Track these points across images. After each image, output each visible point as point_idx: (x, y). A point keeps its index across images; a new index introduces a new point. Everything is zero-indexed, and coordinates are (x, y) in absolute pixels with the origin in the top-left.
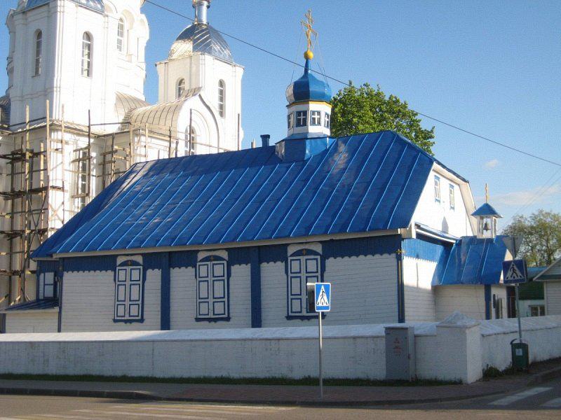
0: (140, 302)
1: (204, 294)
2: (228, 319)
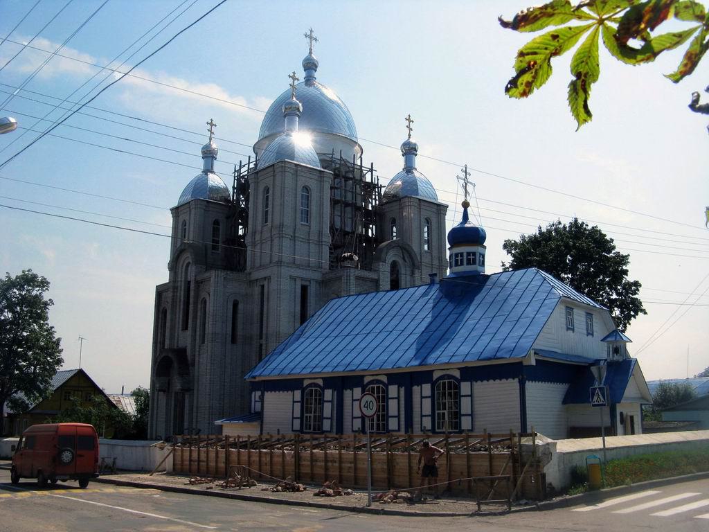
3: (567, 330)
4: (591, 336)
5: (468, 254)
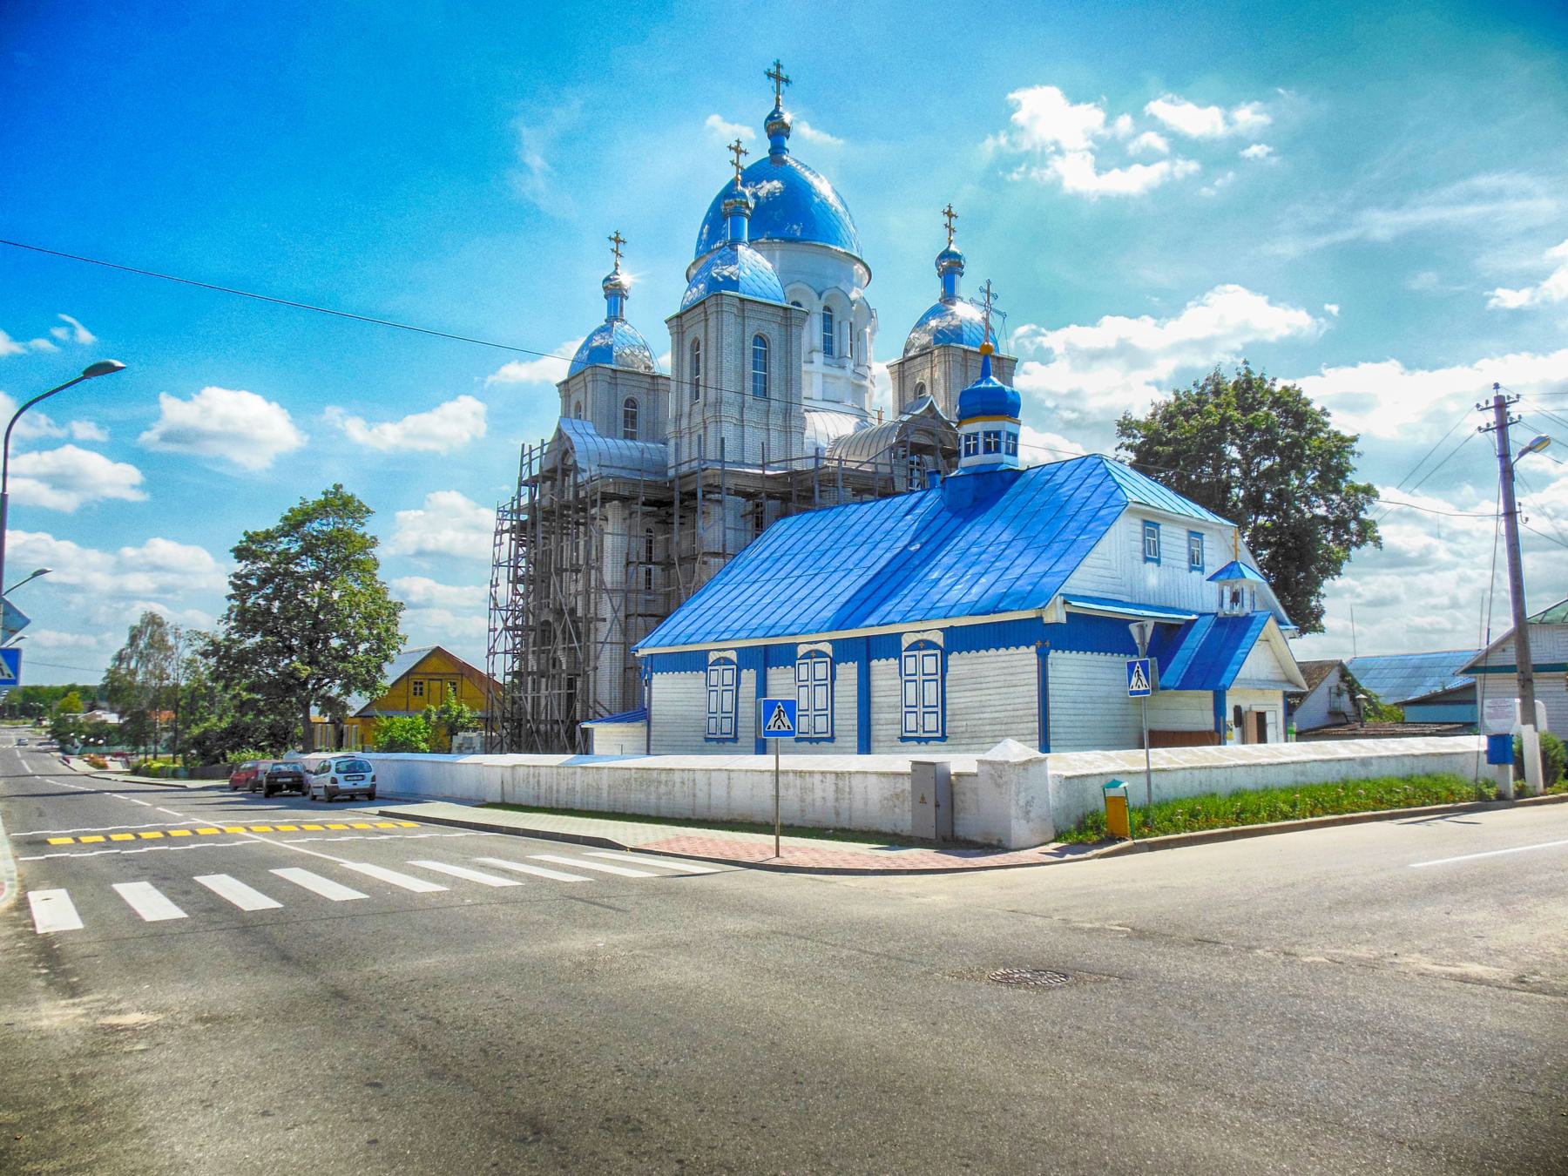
0: (733, 715)
1: (911, 700)
2: (832, 739)
3: (1190, 572)
4: (1155, 565)
5: (987, 434)
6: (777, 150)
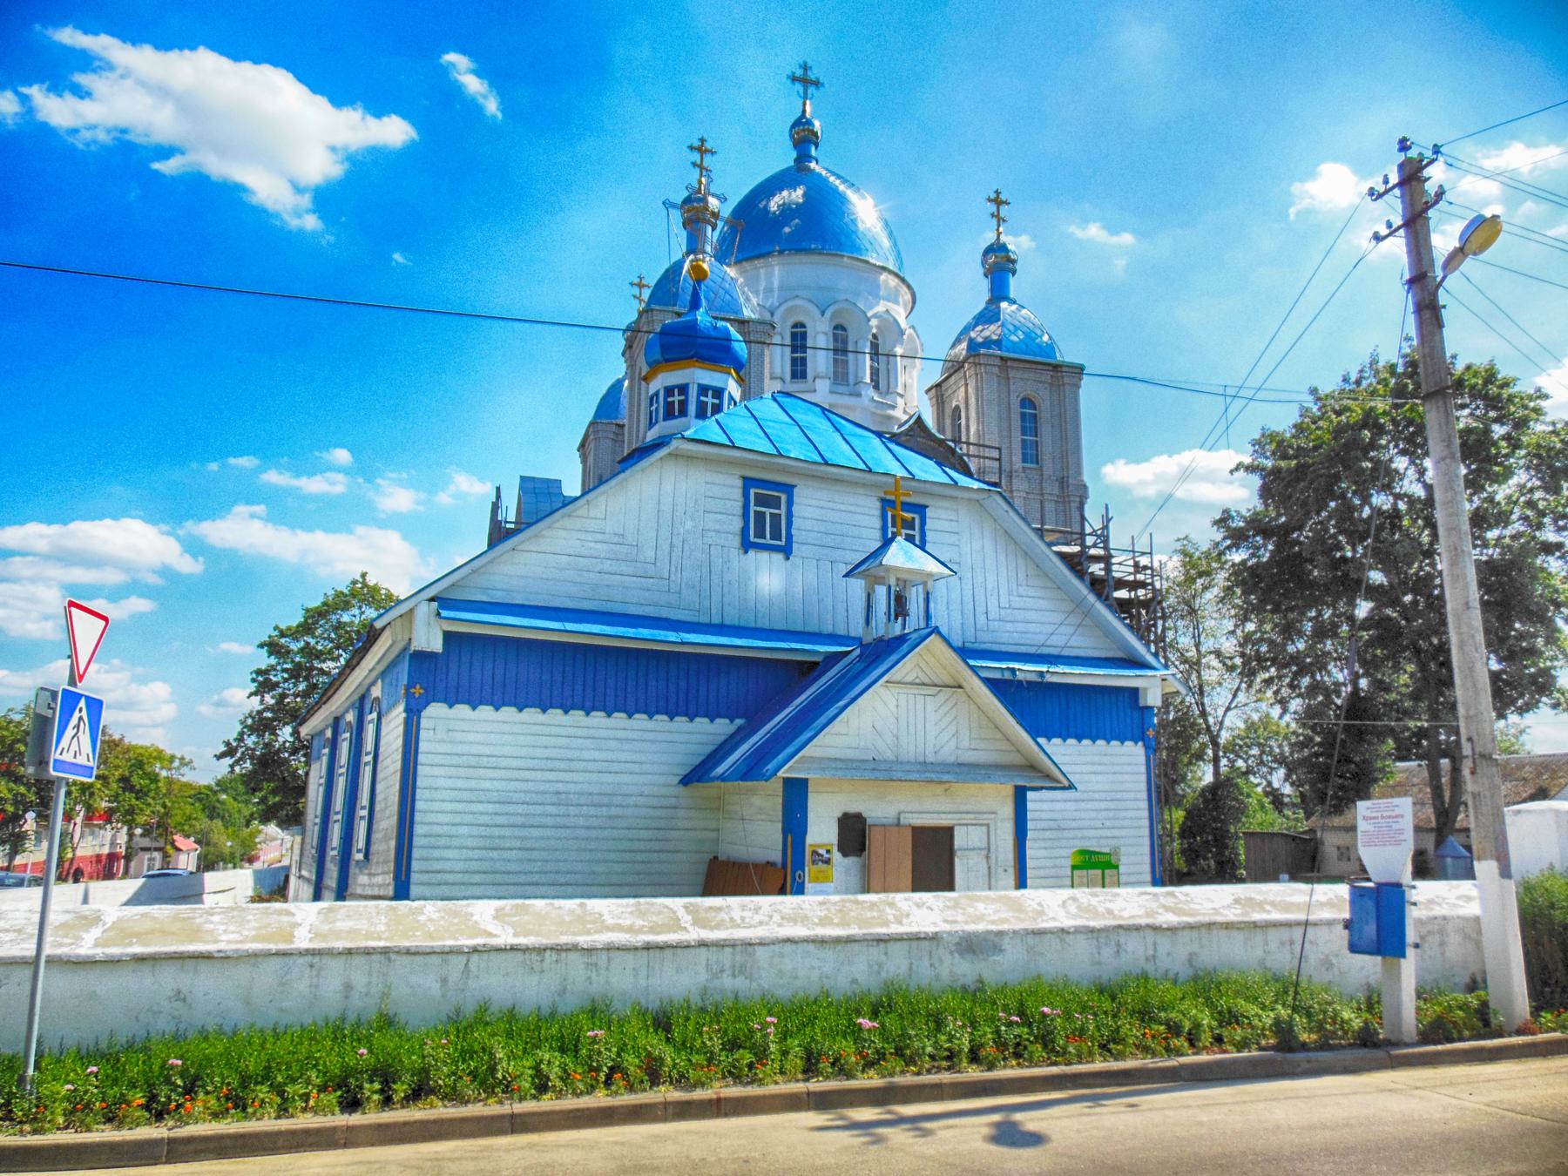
4: (779, 557)
6: (803, 157)
